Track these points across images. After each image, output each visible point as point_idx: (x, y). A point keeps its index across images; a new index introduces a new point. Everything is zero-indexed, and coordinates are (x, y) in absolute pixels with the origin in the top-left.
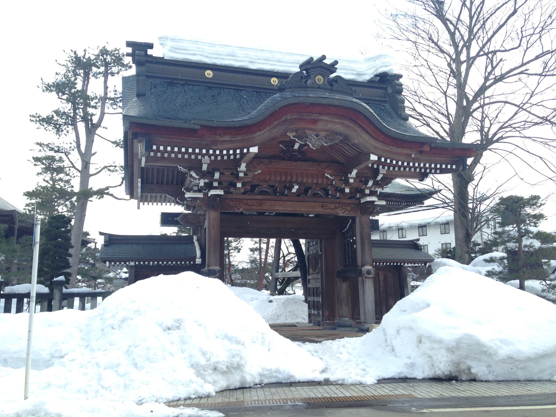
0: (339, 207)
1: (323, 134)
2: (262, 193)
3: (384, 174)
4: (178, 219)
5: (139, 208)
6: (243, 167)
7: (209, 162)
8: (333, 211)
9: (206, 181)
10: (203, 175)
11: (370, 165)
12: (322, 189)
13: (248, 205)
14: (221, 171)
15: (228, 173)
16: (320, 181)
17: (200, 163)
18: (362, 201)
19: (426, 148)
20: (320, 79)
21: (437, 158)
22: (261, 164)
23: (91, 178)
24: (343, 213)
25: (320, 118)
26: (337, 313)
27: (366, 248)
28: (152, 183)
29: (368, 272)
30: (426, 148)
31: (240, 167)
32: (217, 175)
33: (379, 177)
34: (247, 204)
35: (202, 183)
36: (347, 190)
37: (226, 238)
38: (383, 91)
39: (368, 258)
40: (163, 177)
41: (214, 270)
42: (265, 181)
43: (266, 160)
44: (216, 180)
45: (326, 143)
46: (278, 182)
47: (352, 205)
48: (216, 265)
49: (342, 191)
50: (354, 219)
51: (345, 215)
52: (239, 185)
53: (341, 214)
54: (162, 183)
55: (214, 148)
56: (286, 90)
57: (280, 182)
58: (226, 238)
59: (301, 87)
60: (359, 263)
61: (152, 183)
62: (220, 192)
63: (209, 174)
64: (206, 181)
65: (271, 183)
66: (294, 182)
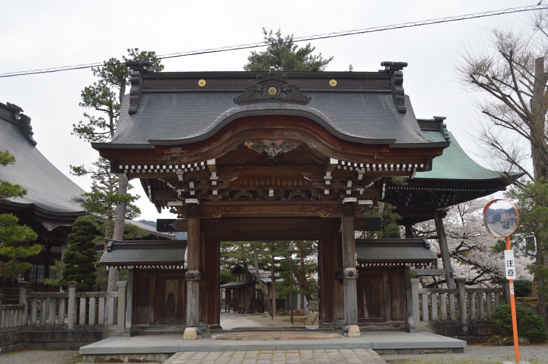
0: (321, 209)
4: (173, 225)
6: (214, 176)
7: (364, 173)
9: (183, 190)
10: (179, 185)
12: (304, 191)
14: (198, 180)
17: (357, 174)
29: (351, 274)
31: (325, 175)
32: (192, 185)
35: (179, 192)
37: (315, 244)
43: (241, 167)
44: (192, 189)
48: (195, 269)
51: (327, 216)
52: (327, 192)
53: (323, 216)
58: (315, 244)
63: (184, 184)
64: (183, 190)
65: (250, 189)
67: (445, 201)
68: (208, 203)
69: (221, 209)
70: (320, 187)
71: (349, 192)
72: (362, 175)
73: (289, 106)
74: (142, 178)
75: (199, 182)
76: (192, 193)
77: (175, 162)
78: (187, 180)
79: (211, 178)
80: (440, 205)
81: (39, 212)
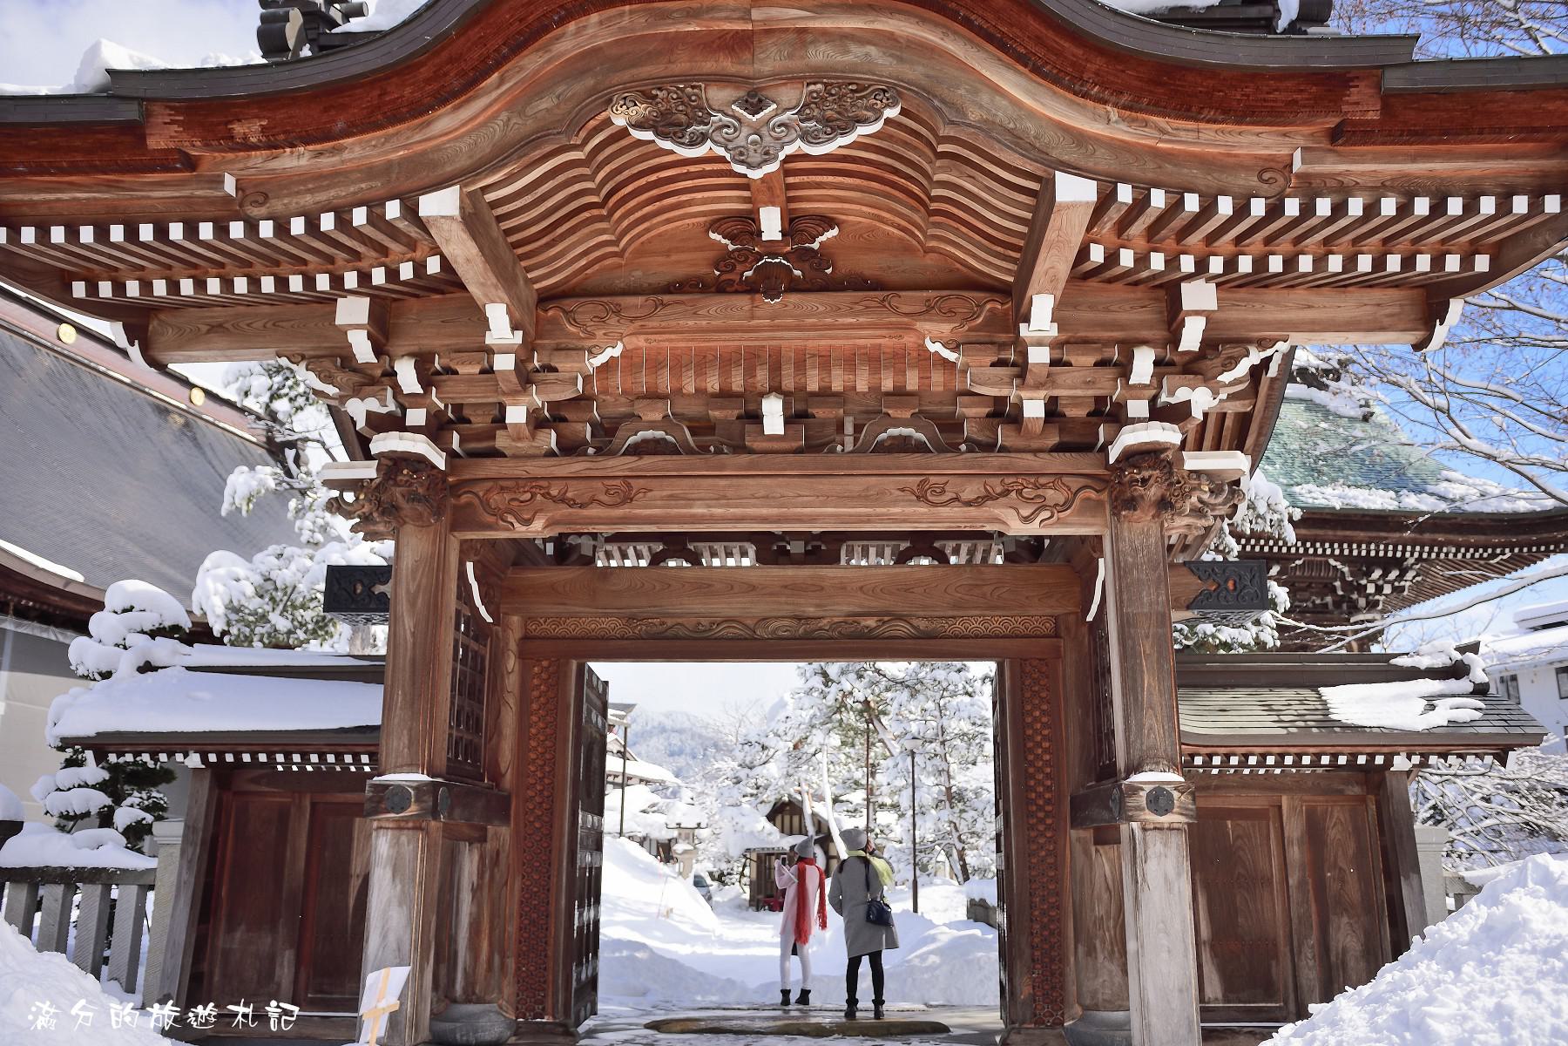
0: (1006, 493)
3: (1208, 315)
8: (973, 511)
13: (572, 503)
16: (912, 382)
19: (1363, 105)
21: (1440, 167)
22: (613, 320)
24: (1026, 520)
26: (1073, 989)
29: (1159, 799)
30: (1363, 105)
31: (1027, 320)
33: (1192, 336)
36: (1034, 409)
41: (400, 789)
42: (654, 396)
43: (640, 300)
47: (1075, 484)
48: (412, 766)
49: (1005, 413)
51: (1034, 529)
57: (725, 395)
60: (1121, 763)
67: (1379, 590)
68: (491, 468)
69: (547, 495)
70: (1004, 392)
71: (1138, 408)
74: (132, 321)
77: (263, 210)
80: (1362, 602)
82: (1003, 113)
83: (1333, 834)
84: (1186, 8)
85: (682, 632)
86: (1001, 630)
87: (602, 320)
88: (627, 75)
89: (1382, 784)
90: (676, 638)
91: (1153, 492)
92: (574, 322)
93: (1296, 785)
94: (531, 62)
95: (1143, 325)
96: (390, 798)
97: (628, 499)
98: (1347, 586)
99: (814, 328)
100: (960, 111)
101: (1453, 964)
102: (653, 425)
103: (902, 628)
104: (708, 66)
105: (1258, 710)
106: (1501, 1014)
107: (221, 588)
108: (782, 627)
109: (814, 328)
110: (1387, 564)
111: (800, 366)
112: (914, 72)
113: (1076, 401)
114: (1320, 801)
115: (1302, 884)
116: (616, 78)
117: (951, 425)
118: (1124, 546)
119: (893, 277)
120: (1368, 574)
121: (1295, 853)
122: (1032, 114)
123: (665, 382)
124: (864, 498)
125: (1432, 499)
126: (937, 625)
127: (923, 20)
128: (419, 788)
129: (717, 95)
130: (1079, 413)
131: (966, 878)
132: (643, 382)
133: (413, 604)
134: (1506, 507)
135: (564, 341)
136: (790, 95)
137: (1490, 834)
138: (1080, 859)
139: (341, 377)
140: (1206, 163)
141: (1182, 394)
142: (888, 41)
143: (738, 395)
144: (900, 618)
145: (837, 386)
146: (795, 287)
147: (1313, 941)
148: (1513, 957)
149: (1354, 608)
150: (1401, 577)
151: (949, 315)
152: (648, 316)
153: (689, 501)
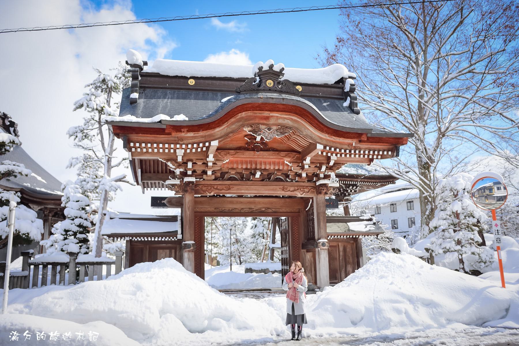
0: (298, 189)
1: (275, 128)
2: (231, 179)
4: (165, 202)
5: (143, 193)
6: (211, 158)
8: (292, 193)
9: (182, 170)
10: (179, 165)
11: (320, 153)
13: (219, 190)
14: (194, 161)
15: (200, 163)
16: (281, 168)
18: (318, 183)
19: (364, 138)
20: (270, 83)
21: (374, 146)
22: (228, 155)
23: (112, 169)
24: (301, 194)
25: (271, 114)
27: (322, 224)
28: (150, 172)
29: (323, 244)
33: (331, 164)
34: (217, 189)
35: (178, 171)
36: (304, 175)
38: (340, 90)
39: (323, 233)
40: (158, 167)
41: (189, 245)
42: (233, 169)
43: (233, 151)
44: (190, 169)
45: (277, 135)
46: (244, 169)
47: (310, 188)
48: (191, 240)
49: (300, 175)
50: (312, 198)
51: (303, 196)
54: (158, 172)
55: (181, 143)
56: (242, 93)
57: (246, 169)
59: (254, 90)
60: (316, 237)
61: (150, 172)
62: (193, 179)
66: (258, 169)
67: (351, 191)
69: (214, 188)
72: (334, 161)
73: (284, 96)
75: (195, 163)
76: (190, 172)
78: (185, 161)
79: (208, 159)
81: (27, 195)
82: (309, 133)
83: (348, 250)
84: (327, 84)
85: (226, 211)
86: (285, 211)
87: (226, 155)
88: (247, 122)
89: (357, 240)
90: (225, 212)
91: (324, 191)
92: (220, 155)
93: (342, 241)
94: (233, 120)
95: (323, 160)
96: (187, 246)
97: (229, 189)
98: (343, 190)
99: (265, 158)
100: (302, 132)
101: (372, 264)
102: (233, 174)
103: (270, 211)
104: (262, 122)
105: (337, 227)
106: (377, 269)
107: (73, 191)
108: (247, 210)
109: (265, 158)
110: (353, 185)
111: (261, 164)
112: (296, 125)
113: (310, 173)
114: (346, 244)
115: (342, 259)
116: (246, 123)
117: (287, 176)
118: (318, 200)
119: (279, 148)
120: (349, 187)
121: (341, 253)
122: (314, 133)
123: (235, 166)
124: (273, 190)
125: (364, 171)
126: (278, 210)
127: (298, 118)
128: (193, 244)
129: (262, 127)
130: (311, 175)
131: (241, 263)
132: (230, 166)
133: (189, 209)
134: (381, 174)
135: (218, 159)
136: (275, 128)
137: (372, 250)
138: (303, 255)
139: (176, 165)
140: (340, 143)
141: (329, 173)
142: (292, 120)
143: (249, 169)
144: (269, 208)
145: (267, 168)
146: (262, 150)
147: (344, 269)
148: (378, 263)
149: (345, 195)
150: (356, 188)
151: (290, 157)
152: (235, 154)
153: (241, 190)
